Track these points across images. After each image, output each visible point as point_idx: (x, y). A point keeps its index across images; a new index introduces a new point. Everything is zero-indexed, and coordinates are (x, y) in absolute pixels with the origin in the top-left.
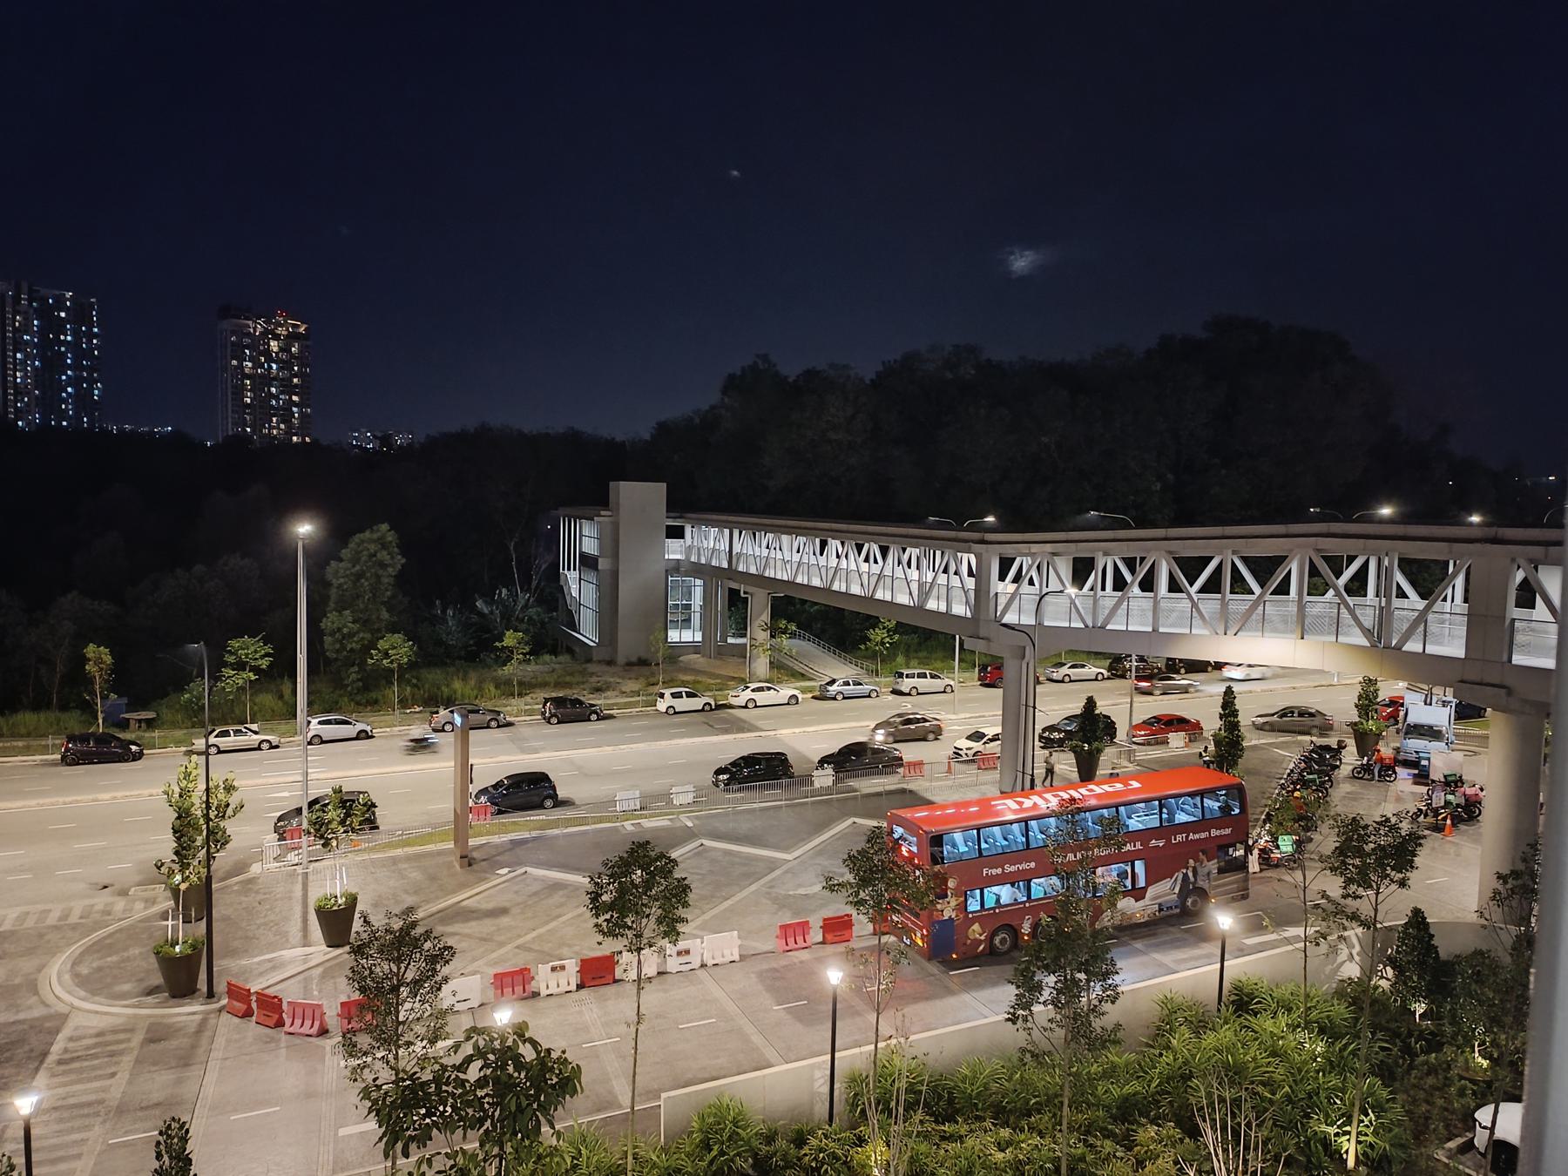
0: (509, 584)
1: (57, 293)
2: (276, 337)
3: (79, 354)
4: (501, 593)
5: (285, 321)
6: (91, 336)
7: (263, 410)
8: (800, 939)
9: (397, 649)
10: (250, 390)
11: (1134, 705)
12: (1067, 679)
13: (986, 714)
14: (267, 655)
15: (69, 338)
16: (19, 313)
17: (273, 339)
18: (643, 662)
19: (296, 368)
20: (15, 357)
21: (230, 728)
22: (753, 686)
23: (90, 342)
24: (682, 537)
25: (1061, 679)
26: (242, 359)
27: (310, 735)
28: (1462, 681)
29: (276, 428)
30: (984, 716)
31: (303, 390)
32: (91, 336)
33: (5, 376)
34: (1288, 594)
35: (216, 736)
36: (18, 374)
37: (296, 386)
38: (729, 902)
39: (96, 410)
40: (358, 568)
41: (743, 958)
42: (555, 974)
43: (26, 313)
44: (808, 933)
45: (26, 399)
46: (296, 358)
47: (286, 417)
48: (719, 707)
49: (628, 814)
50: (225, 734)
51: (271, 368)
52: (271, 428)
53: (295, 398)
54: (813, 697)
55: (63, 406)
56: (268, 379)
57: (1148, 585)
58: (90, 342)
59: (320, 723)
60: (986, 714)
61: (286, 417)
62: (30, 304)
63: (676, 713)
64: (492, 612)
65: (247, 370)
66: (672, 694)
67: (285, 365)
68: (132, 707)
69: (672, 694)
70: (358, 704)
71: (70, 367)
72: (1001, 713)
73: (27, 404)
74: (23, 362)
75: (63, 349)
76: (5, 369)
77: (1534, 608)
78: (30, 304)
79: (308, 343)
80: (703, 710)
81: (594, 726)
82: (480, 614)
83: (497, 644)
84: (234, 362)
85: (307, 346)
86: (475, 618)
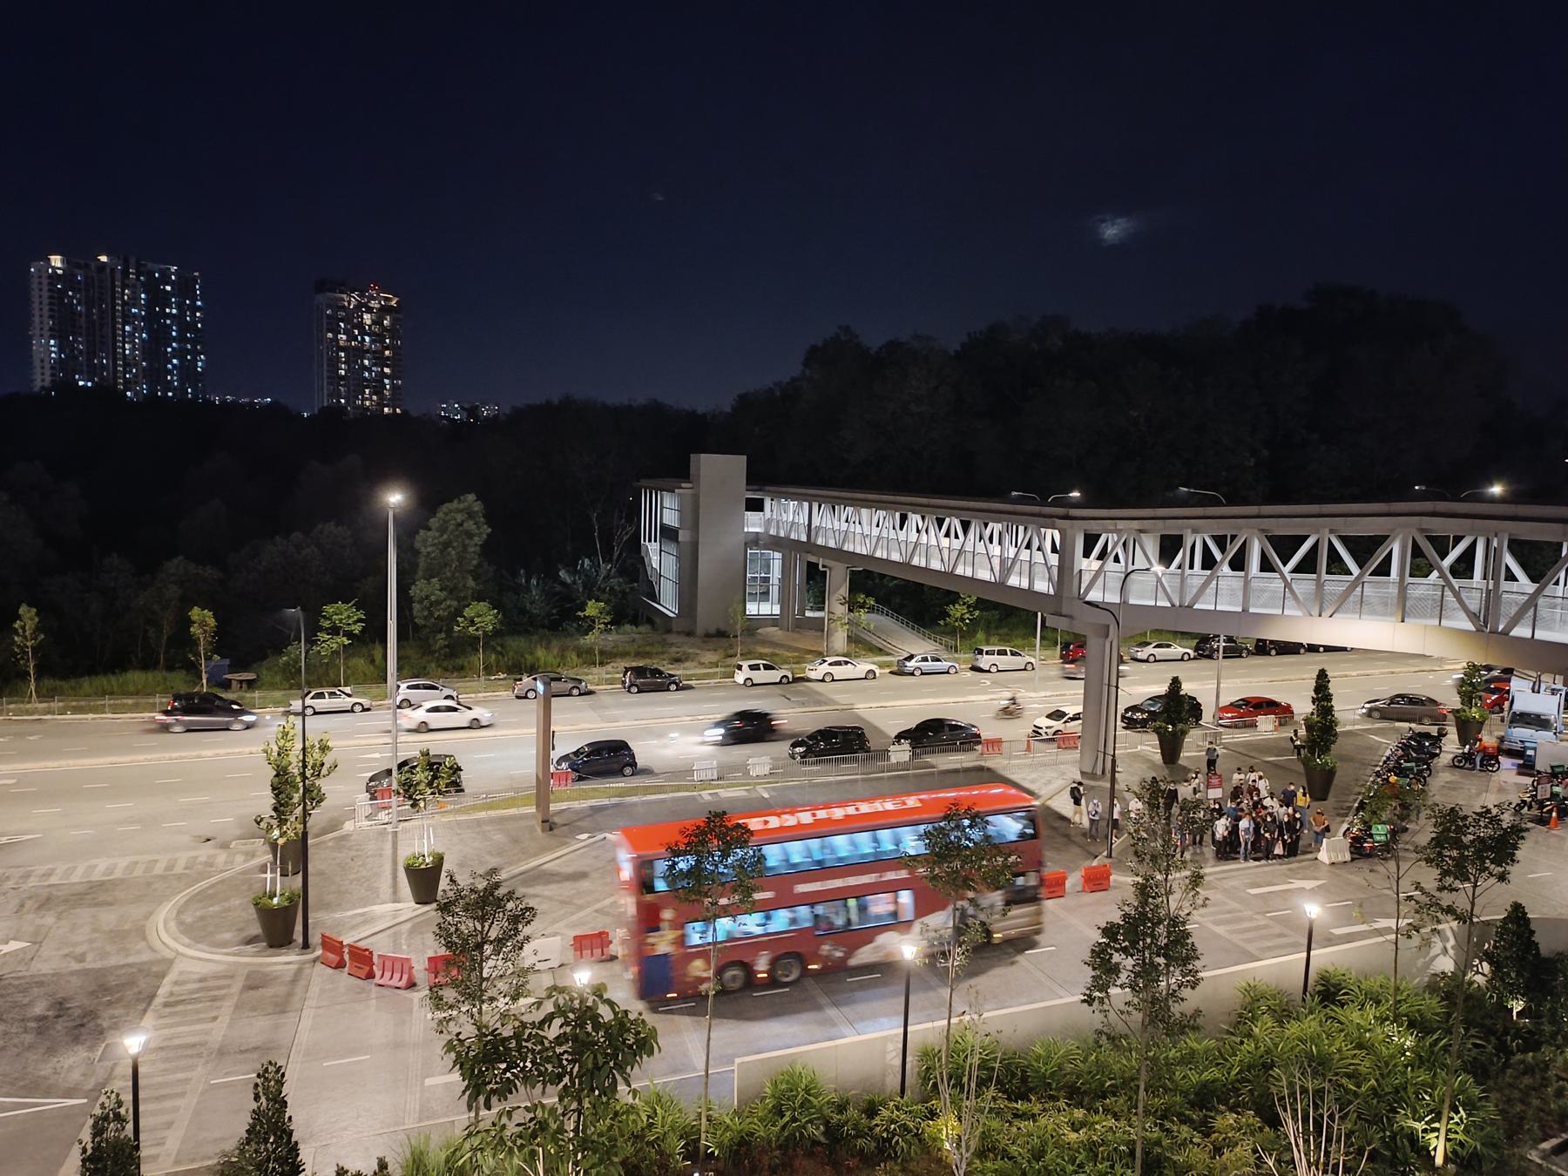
0: (591, 554)
1: (163, 267)
2: (370, 310)
3: (184, 328)
4: (583, 563)
6: (195, 309)
7: (356, 383)
9: (482, 617)
10: (344, 363)
12: (1152, 659)
13: (1067, 692)
14: (360, 620)
15: (174, 311)
17: (367, 312)
19: (388, 341)
21: (326, 691)
22: (830, 660)
25: (1145, 658)
26: (336, 332)
29: (368, 399)
31: (394, 362)
32: (195, 309)
33: (115, 348)
35: (312, 698)
36: (127, 346)
37: (388, 358)
40: (445, 536)
45: (134, 371)
46: (387, 331)
47: (378, 389)
48: (796, 680)
49: (705, 784)
50: (320, 696)
51: (364, 340)
52: (364, 399)
53: (387, 370)
54: (891, 673)
55: (169, 378)
56: (360, 352)
57: (1238, 563)
59: (409, 687)
61: (378, 389)
63: (753, 685)
64: (574, 582)
65: (341, 343)
67: (378, 337)
70: (446, 670)
71: (174, 339)
73: (135, 376)
74: (132, 335)
75: (168, 322)
76: (115, 341)
78: (138, 279)
80: (780, 682)
82: (563, 583)
83: (579, 613)
84: (330, 335)
85: (399, 320)
86: (558, 588)
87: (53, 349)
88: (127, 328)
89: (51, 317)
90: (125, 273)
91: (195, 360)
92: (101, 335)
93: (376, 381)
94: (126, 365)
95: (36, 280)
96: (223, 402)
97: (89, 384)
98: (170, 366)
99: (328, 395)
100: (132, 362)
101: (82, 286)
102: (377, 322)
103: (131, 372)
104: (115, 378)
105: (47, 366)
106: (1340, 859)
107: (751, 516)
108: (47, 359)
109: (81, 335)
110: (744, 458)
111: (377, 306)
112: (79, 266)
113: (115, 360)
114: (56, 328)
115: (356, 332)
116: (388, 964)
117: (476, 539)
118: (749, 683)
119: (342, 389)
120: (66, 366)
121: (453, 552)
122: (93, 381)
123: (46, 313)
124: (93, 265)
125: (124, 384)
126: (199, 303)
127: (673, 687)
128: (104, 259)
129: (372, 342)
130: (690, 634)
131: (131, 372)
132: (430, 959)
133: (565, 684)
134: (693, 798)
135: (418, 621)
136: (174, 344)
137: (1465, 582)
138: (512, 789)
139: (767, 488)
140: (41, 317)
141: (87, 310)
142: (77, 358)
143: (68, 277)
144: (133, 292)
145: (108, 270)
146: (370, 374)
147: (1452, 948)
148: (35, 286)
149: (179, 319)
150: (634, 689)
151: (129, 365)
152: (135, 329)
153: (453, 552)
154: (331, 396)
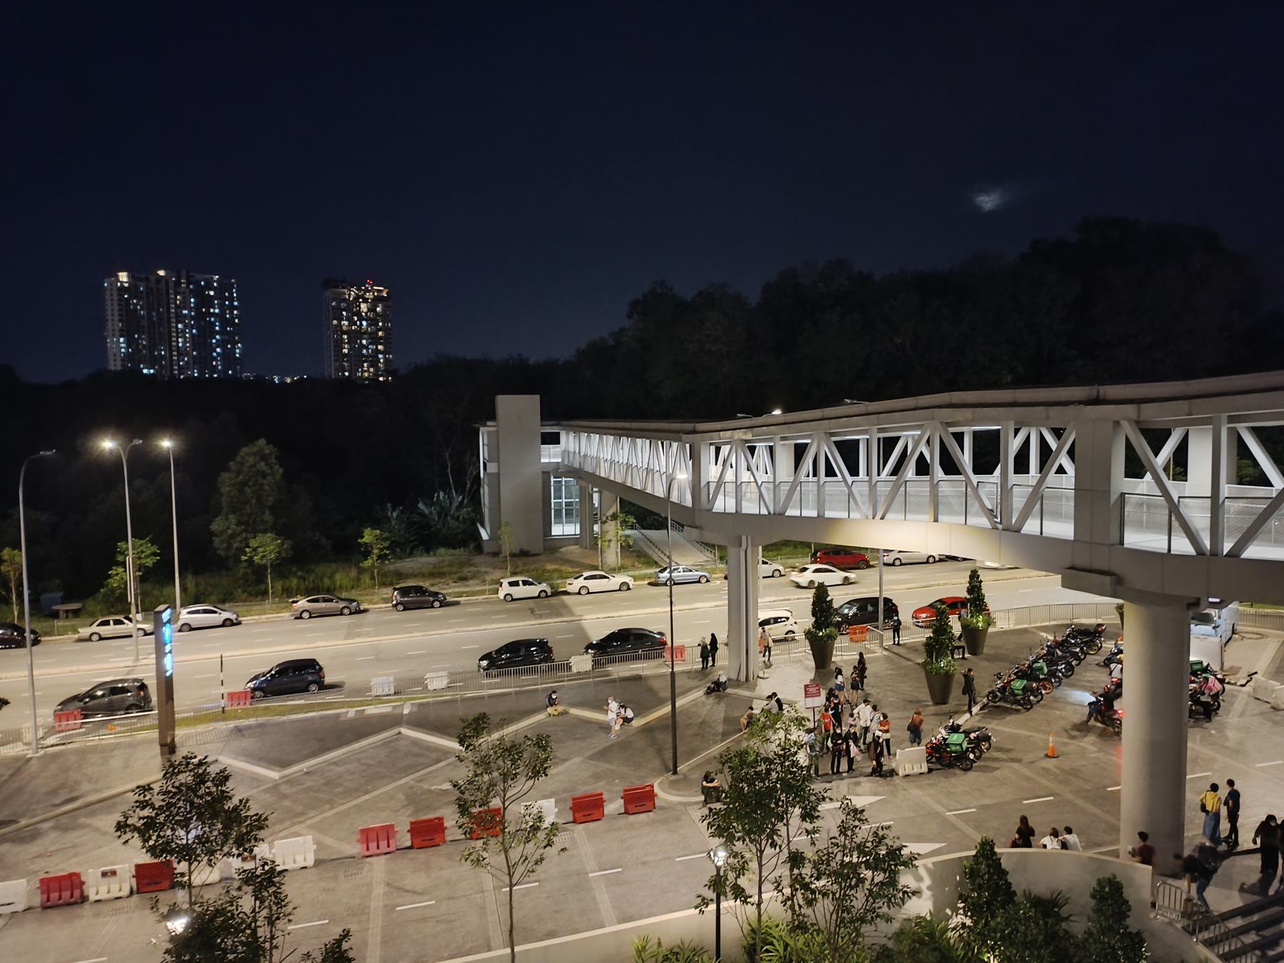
0: (445, 487)
1: (208, 276)
2: (365, 301)
3: (225, 322)
4: (438, 496)
5: (372, 287)
6: (232, 308)
7: (357, 358)
8: (383, 844)
9: (266, 548)
10: (347, 343)
11: (878, 589)
12: (898, 562)
13: (792, 597)
14: (155, 554)
15: (217, 311)
16: (179, 294)
17: (363, 302)
18: (524, 554)
19: (380, 324)
20: (177, 328)
21: (111, 618)
22: (586, 574)
23: (231, 313)
24: (558, 443)
25: (891, 562)
26: (340, 319)
27: (180, 623)
28: (1072, 568)
29: (366, 371)
30: (801, 598)
31: (386, 341)
32: (232, 308)
33: (171, 341)
34: (858, 475)
35: (98, 625)
36: (180, 340)
37: (381, 338)
38: (367, 797)
39: (239, 364)
40: (241, 477)
41: (318, 863)
42: (106, 879)
43: (184, 293)
44: (394, 837)
45: (186, 359)
46: (380, 316)
47: (374, 363)
48: (554, 594)
49: (378, 699)
50: (106, 623)
51: (361, 324)
52: (363, 372)
53: (380, 347)
54: (649, 584)
55: (214, 363)
56: (360, 334)
57: (951, 467)
58: (231, 313)
59: (189, 613)
60: (792, 597)
61: (374, 363)
62: (188, 287)
63: (513, 600)
64: (431, 513)
65: (344, 328)
66: (509, 583)
67: (372, 322)
68: (65, 600)
69: (509, 583)
70: (250, 594)
71: (218, 333)
72: (727, 602)
73: (187, 362)
74: (183, 331)
75: (213, 319)
76: (170, 337)
77: (1186, 481)
78: (188, 287)
79: (390, 304)
80: (539, 597)
81: (437, 612)
82: (422, 514)
83: (359, 540)
84: (335, 322)
85: (388, 307)
86: (416, 518)
87: (122, 345)
88: (180, 326)
89: (120, 320)
90: (178, 283)
91: (234, 348)
92: (160, 333)
93: (371, 356)
94: (179, 355)
95: (108, 293)
96: (283, 383)
97: (152, 371)
98: (215, 354)
99: (335, 370)
100: (184, 353)
101: (144, 295)
102: (371, 310)
103: (183, 360)
104: (172, 366)
105: (119, 359)
106: (917, 770)
107: (546, 449)
108: (118, 354)
109: (144, 333)
110: (538, 397)
111: (372, 297)
112: (141, 280)
113: (171, 352)
114: (125, 329)
115: (356, 318)
116: (373, 835)
117: (269, 478)
118: (509, 598)
119: (346, 364)
120: (134, 358)
121: (249, 491)
122: (154, 369)
123: (116, 318)
124: (152, 278)
125: (178, 370)
126: (236, 303)
127: (437, 604)
128: (162, 273)
129: (368, 325)
130: (496, 554)
131: (183, 360)
132: (42, 881)
133: (337, 604)
134: (338, 716)
135: (222, 553)
136: (218, 337)
137: (855, 478)
138: (194, 711)
139: (564, 423)
140: (114, 322)
141: (148, 313)
142: (141, 351)
143: (132, 289)
144: (184, 298)
145: (164, 281)
146: (368, 351)
147: (929, 888)
148: (108, 297)
149: (221, 317)
150: (401, 607)
151: (182, 354)
152: (186, 326)
153: (249, 491)
154: (337, 370)
